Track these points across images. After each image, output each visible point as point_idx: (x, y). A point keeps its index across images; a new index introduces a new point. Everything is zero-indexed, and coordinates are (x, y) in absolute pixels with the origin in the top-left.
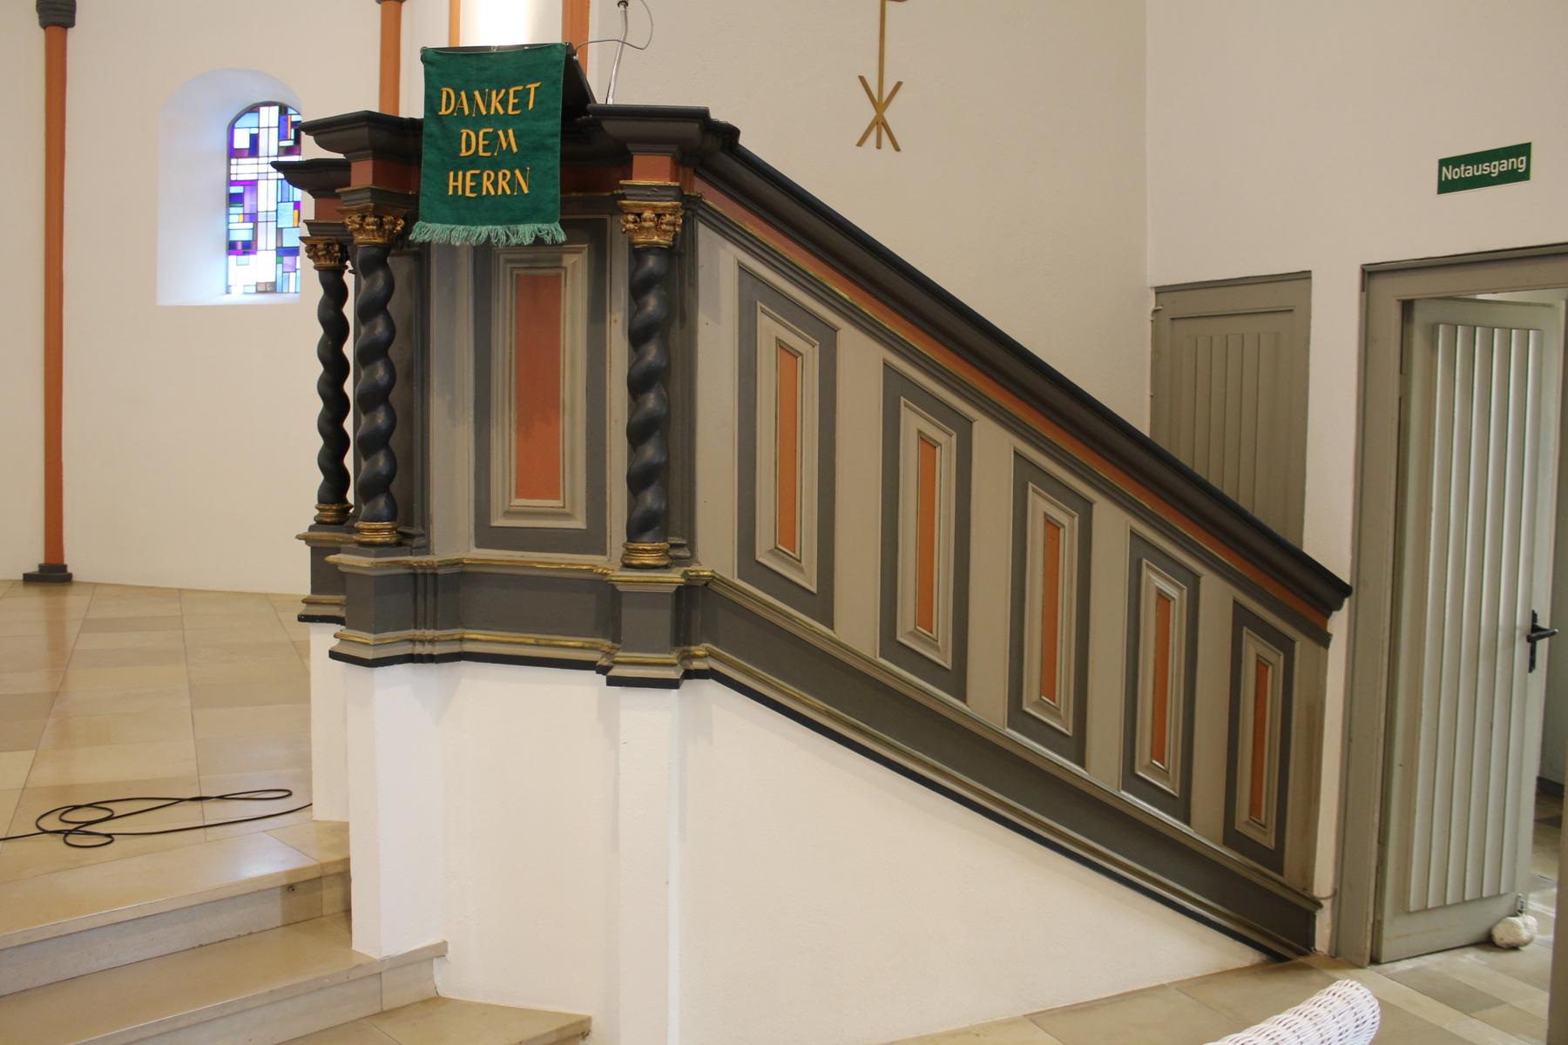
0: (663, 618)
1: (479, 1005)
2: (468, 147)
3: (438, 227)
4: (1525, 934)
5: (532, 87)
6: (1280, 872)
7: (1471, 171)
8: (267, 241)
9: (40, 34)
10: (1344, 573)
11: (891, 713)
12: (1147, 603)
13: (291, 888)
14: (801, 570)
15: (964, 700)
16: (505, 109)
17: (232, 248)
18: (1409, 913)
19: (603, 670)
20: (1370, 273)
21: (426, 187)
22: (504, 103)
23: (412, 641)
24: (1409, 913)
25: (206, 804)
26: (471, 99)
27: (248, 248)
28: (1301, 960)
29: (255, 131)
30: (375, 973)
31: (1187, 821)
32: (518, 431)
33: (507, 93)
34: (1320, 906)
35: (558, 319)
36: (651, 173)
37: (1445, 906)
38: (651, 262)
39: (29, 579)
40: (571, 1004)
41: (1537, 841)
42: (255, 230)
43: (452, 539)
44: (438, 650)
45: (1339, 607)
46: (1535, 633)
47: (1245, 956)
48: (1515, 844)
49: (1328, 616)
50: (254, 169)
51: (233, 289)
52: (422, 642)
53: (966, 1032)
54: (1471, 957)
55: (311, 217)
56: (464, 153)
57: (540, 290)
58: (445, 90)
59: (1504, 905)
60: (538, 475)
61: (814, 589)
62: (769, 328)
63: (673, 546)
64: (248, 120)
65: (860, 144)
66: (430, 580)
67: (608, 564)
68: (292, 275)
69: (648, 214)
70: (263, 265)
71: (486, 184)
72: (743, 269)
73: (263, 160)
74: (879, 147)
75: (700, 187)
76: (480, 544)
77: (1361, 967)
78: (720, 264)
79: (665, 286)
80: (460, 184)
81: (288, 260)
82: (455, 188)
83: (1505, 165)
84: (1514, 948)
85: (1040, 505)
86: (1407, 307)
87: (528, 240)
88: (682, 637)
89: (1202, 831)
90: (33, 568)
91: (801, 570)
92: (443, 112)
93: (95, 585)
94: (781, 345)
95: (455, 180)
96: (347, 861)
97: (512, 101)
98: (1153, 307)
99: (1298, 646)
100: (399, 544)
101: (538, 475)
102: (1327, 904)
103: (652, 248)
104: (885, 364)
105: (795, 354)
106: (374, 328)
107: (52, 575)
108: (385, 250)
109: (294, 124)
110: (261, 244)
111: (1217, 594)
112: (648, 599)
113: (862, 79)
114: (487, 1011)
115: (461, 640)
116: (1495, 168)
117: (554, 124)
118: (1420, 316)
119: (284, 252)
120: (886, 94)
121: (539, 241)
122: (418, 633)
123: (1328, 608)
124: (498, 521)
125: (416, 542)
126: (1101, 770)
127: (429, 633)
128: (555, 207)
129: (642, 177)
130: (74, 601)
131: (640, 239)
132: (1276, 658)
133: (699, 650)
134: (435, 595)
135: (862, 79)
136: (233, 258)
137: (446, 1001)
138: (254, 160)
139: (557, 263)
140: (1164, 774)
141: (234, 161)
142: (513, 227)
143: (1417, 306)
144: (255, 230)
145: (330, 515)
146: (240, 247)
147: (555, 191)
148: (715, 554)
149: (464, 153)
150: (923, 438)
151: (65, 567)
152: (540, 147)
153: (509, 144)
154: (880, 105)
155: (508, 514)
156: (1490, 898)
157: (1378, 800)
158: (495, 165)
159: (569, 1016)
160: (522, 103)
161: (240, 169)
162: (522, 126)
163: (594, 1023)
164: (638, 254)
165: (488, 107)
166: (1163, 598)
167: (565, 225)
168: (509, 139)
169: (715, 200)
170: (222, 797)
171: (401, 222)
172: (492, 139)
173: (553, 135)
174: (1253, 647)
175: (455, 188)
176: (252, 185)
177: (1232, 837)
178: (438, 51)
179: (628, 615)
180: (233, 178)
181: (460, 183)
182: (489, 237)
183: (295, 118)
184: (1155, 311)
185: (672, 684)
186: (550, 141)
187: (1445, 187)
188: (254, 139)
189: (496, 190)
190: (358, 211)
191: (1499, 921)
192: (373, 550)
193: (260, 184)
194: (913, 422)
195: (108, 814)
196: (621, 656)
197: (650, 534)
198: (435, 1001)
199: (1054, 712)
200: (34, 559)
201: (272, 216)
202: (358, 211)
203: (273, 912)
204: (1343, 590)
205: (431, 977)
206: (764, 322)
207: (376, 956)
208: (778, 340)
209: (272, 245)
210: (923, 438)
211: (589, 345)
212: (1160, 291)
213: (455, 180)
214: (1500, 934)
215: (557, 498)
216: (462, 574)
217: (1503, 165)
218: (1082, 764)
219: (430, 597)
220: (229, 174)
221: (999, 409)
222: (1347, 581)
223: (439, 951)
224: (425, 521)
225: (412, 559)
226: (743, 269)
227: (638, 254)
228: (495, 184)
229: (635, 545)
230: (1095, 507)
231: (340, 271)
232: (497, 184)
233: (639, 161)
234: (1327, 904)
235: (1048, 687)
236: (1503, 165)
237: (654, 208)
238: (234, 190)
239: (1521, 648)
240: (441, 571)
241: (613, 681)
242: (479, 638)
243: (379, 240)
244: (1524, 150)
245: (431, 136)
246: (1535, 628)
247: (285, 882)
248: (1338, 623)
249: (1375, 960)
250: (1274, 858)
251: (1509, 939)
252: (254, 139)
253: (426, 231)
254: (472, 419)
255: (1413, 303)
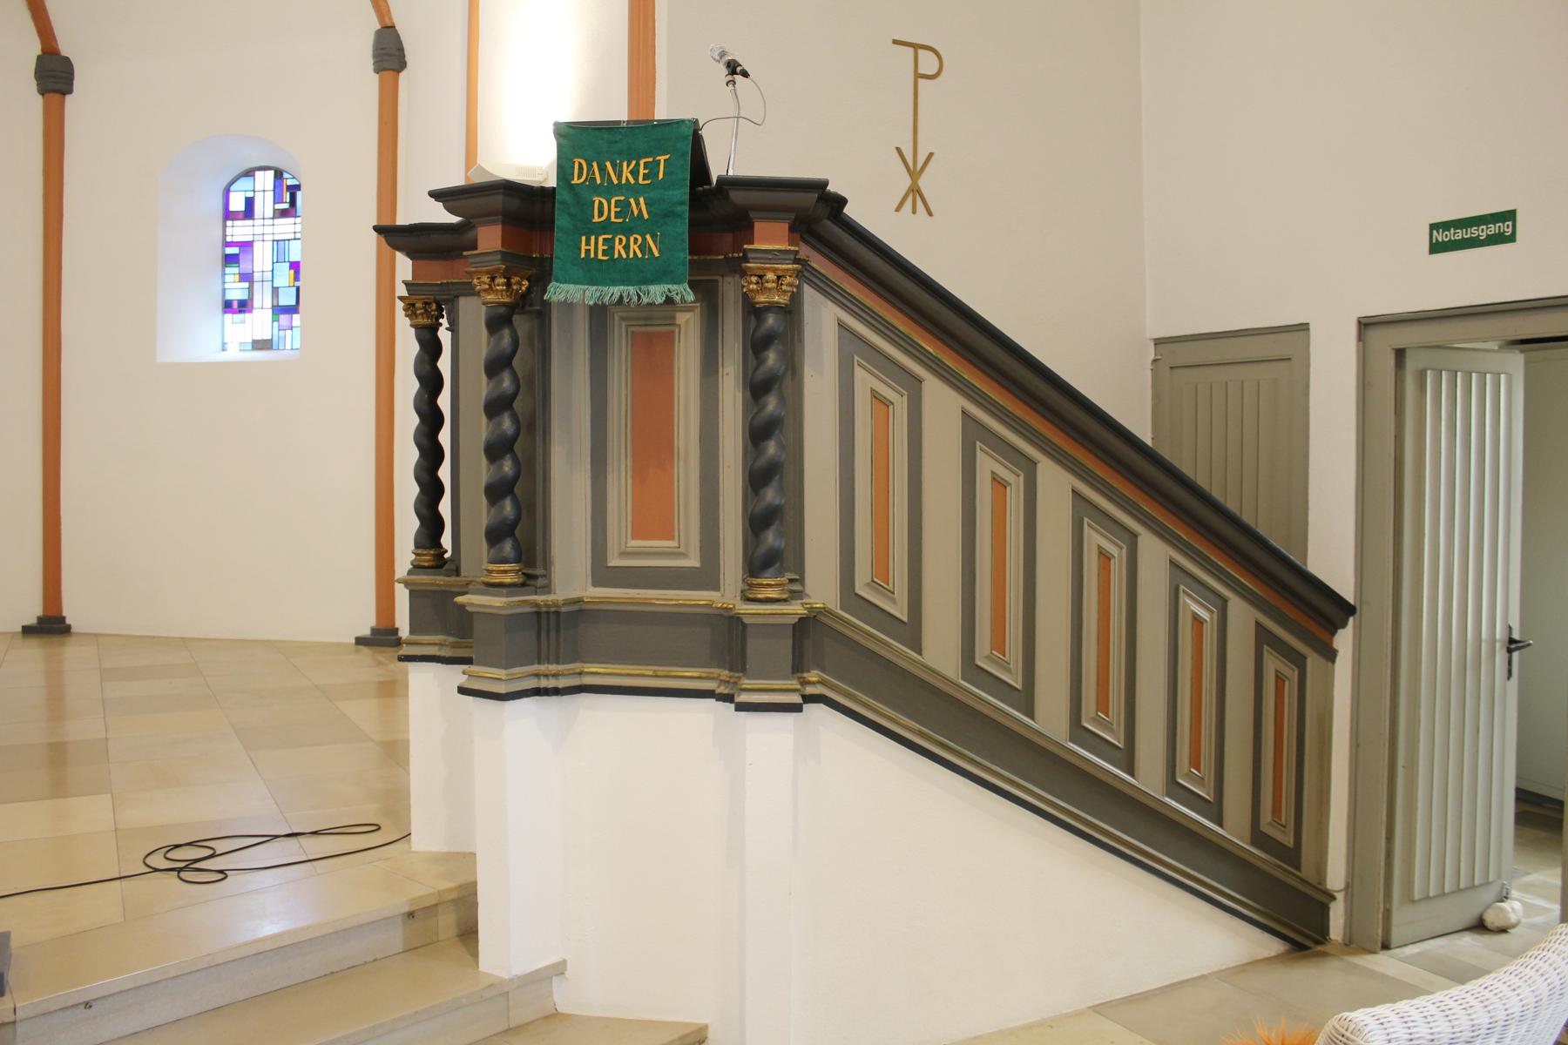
0: (785, 646)
1: (598, 1018)
2: (601, 214)
3: (572, 287)
4: (1513, 918)
5: (662, 158)
6: (1298, 868)
7: (1460, 234)
8: (262, 300)
9: (38, 100)
10: (1347, 592)
11: (966, 729)
12: (1179, 624)
13: (411, 915)
14: (894, 601)
15: (1032, 718)
16: (636, 179)
17: (228, 306)
18: (1413, 902)
19: (728, 698)
20: (1366, 325)
21: (560, 251)
22: (635, 173)
23: (537, 675)
24: (1413, 902)
25: (302, 839)
26: (602, 169)
27: (244, 306)
28: (1319, 948)
29: (250, 194)
30: (502, 992)
31: (1221, 825)
32: (633, 477)
33: (638, 164)
34: (1334, 898)
35: (671, 374)
36: (770, 238)
37: (1443, 894)
38: (771, 320)
39: (27, 631)
40: (689, 1015)
41: (1517, 835)
42: (251, 290)
43: (571, 579)
44: (562, 683)
45: (1344, 625)
46: (1512, 645)
47: (1273, 946)
48: (1500, 837)
49: (1333, 633)
50: (250, 230)
51: (229, 347)
52: (546, 676)
53: (1040, 1024)
54: (1469, 941)
55: (409, 278)
56: (596, 219)
57: (652, 334)
58: (577, 161)
59: (1492, 892)
60: (654, 517)
61: (905, 619)
62: (865, 381)
63: (791, 581)
64: (244, 184)
65: (898, 210)
66: (553, 618)
67: (728, 594)
68: (289, 332)
69: (770, 276)
70: (260, 323)
71: (618, 247)
72: (841, 325)
73: (257, 222)
74: (914, 212)
75: (805, 251)
76: (596, 584)
77: (1374, 952)
78: (823, 320)
79: (771, 344)
80: (592, 248)
81: (284, 318)
82: (588, 251)
83: (1493, 229)
84: (1503, 930)
85: (1095, 539)
86: (1400, 354)
87: (660, 300)
88: (798, 667)
89: (1233, 832)
90: (31, 620)
91: (894, 601)
92: (575, 181)
93: (96, 635)
94: (875, 395)
95: (588, 243)
96: (475, 883)
97: (642, 171)
98: (1152, 357)
99: (1309, 661)
100: (523, 585)
101: (654, 517)
102: (1340, 897)
103: (771, 307)
104: (964, 412)
105: (887, 403)
106: (501, 381)
107: (51, 626)
108: (512, 309)
109: (289, 188)
110: (257, 302)
111: (1242, 616)
112: (771, 630)
113: (898, 150)
114: (607, 1023)
115: (580, 674)
116: (1483, 232)
117: (683, 193)
118: (1411, 365)
119: (279, 310)
120: (919, 165)
121: (669, 301)
122: (543, 668)
123: (1334, 626)
124: (614, 561)
125: (540, 582)
126: (1148, 780)
127: (553, 668)
128: (683, 270)
129: (763, 241)
130: (72, 653)
131: (762, 298)
132: (1292, 673)
133: (813, 676)
134: (558, 631)
135: (898, 150)
136: (228, 316)
137: (566, 1017)
138: (249, 222)
139: (671, 321)
140: (1200, 781)
141: (229, 223)
142: (644, 288)
143: (1408, 354)
144: (251, 290)
145: (427, 560)
146: (235, 305)
147: (684, 255)
148: (822, 590)
149: (596, 219)
150: (995, 478)
151: (63, 619)
152: (669, 214)
153: (640, 211)
154: (914, 174)
155: (624, 554)
156: (1452, 893)
157: (1305, 805)
158: (627, 230)
159: (687, 1025)
160: (651, 174)
161: (236, 231)
162: (652, 195)
163: (711, 1030)
164: (753, 312)
165: (619, 177)
166: (1197, 620)
167: (692, 285)
168: (640, 207)
169: (819, 263)
170: (315, 833)
171: (526, 283)
172: (624, 208)
173: (682, 203)
174: (1272, 663)
175: (588, 251)
176: (247, 246)
177: (1259, 838)
178: (572, 126)
179: (753, 646)
180: (229, 239)
181: (593, 247)
182: (621, 297)
183: (291, 182)
184: (1155, 361)
185: (796, 708)
186: (679, 209)
187: (1435, 248)
188: (250, 202)
189: (628, 253)
190: (487, 272)
191: (1489, 906)
192: (505, 591)
193: (256, 245)
194: (987, 464)
195: (210, 852)
196: (747, 683)
197: (771, 570)
198: (554, 1016)
199: (1108, 726)
200: (32, 612)
201: (268, 276)
202: (487, 272)
203: (395, 939)
204: (1349, 610)
205: (551, 995)
206: (859, 374)
207: (505, 976)
208: (872, 390)
209: (268, 303)
210: (995, 478)
211: (704, 397)
212: (1158, 342)
213: (588, 243)
214: (1491, 919)
215: (671, 538)
216: (580, 611)
217: (1496, 228)
218: (1132, 774)
219: (553, 634)
220: (225, 235)
221: (1058, 449)
222: (1352, 601)
223: (559, 969)
224: (547, 564)
225: (539, 598)
226: (841, 325)
227: (753, 312)
228: (627, 248)
229: (755, 581)
230: (1140, 539)
231: (435, 328)
232: (629, 248)
233: (759, 227)
234: (1340, 897)
235: (1102, 704)
236: (1496, 228)
237: (774, 271)
238: (229, 251)
239: (1500, 656)
240: (563, 609)
241: (742, 707)
242: (597, 672)
243: (507, 300)
244: (1510, 216)
245: (563, 203)
246: (1512, 641)
247: (406, 909)
248: (1344, 640)
249: (1386, 946)
250: (1292, 856)
251: (1499, 923)
252: (250, 202)
253: (558, 292)
254: (589, 466)
255: (1400, 349)
